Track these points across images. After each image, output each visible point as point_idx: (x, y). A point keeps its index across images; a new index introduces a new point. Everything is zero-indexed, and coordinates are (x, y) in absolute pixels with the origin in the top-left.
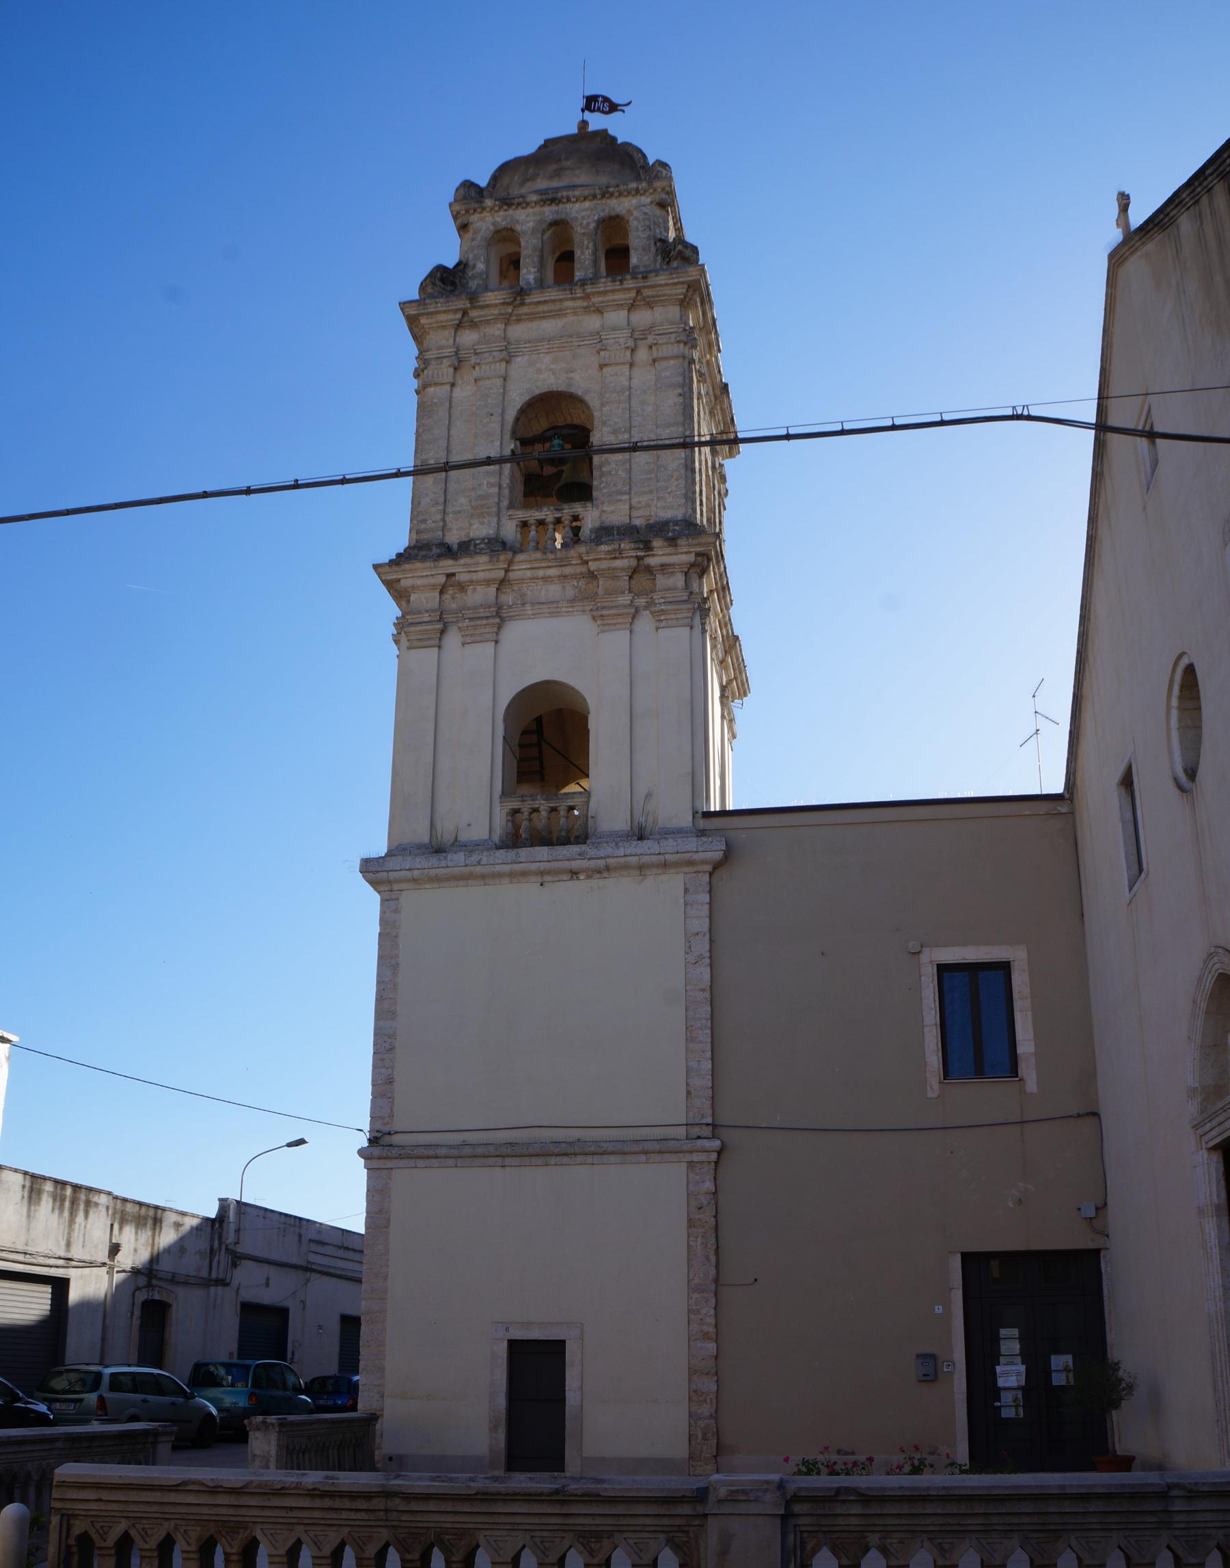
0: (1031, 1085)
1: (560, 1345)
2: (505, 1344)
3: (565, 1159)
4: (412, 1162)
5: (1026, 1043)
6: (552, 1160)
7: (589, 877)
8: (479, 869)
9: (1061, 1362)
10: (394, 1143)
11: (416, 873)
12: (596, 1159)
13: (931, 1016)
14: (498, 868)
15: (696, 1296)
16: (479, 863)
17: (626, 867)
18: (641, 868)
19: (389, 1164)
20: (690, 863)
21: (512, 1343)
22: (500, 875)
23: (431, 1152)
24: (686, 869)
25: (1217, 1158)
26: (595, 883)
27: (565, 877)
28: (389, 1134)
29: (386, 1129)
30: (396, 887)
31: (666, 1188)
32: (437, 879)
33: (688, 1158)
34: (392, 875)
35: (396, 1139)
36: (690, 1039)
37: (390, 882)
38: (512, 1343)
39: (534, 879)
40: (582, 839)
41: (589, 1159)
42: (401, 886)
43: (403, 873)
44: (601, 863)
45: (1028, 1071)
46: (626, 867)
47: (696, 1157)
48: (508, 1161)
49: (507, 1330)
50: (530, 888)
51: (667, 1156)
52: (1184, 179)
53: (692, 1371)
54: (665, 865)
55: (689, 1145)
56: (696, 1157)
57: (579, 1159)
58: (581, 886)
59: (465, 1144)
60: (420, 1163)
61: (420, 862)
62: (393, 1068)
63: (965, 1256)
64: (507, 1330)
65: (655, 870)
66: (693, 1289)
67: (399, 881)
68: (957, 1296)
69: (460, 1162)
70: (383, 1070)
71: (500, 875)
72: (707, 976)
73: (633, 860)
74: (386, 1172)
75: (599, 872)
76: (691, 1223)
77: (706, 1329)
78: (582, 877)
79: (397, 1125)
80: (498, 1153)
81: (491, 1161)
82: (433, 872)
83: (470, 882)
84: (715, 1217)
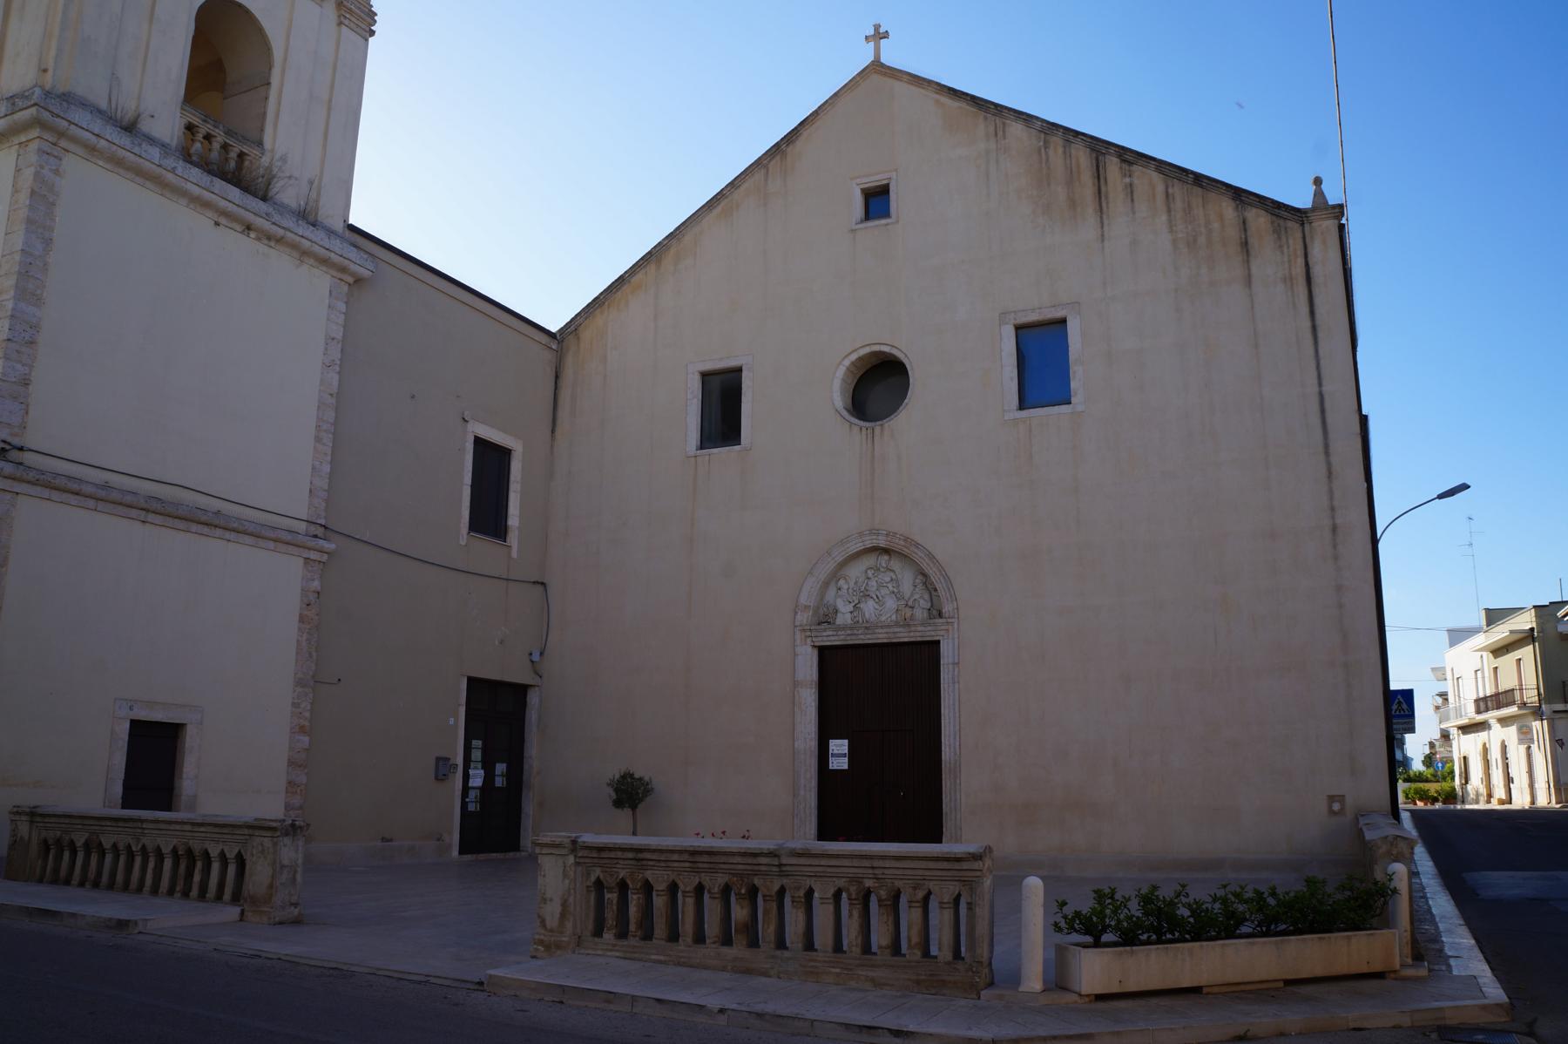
0: (514, 554)
1: (137, 726)
2: (128, 725)
3: (206, 530)
4: (46, 493)
5: (513, 519)
6: (194, 527)
7: (258, 239)
8: (170, 177)
9: (500, 768)
10: (26, 463)
11: (103, 143)
12: (232, 536)
13: (468, 478)
14: (189, 186)
15: (299, 689)
16: (173, 171)
17: (294, 246)
18: (305, 253)
19: (18, 487)
20: (343, 270)
21: (135, 724)
22: (183, 193)
23: (75, 487)
24: (335, 273)
25: (816, 652)
26: (262, 247)
27: (239, 228)
28: (21, 449)
29: (16, 441)
30: (63, 143)
31: (279, 580)
32: (119, 163)
33: (306, 554)
34: (73, 130)
35: (28, 458)
36: (318, 439)
37: (61, 134)
38: (135, 724)
39: (210, 214)
40: (264, 199)
41: (227, 535)
42: (71, 147)
43: (88, 135)
44: (281, 232)
45: (513, 538)
46: (294, 246)
47: (313, 555)
48: (151, 517)
49: (131, 708)
50: (201, 222)
51: (291, 548)
52: (1052, 120)
53: (291, 763)
54: (324, 262)
55: (312, 543)
56: (313, 555)
57: (219, 532)
58: (248, 243)
59: (106, 486)
60: (55, 495)
61: (111, 133)
62: (31, 367)
63: (471, 680)
64: (131, 708)
65: (312, 261)
66: (299, 683)
67: (74, 140)
68: (462, 711)
69: (101, 505)
70: (19, 366)
71: (183, 193)
72: (335, 383)
73: (306, 244)
74: (9, 496)
75: (269, 238)
76: (302, 619)
77: (303, 722)
78: (253, 235)
79: (30, 440)
80: (144, 505)
81: (134, 513)
82: (121, 153)
83: (148, 184)
84: (795, 655)
